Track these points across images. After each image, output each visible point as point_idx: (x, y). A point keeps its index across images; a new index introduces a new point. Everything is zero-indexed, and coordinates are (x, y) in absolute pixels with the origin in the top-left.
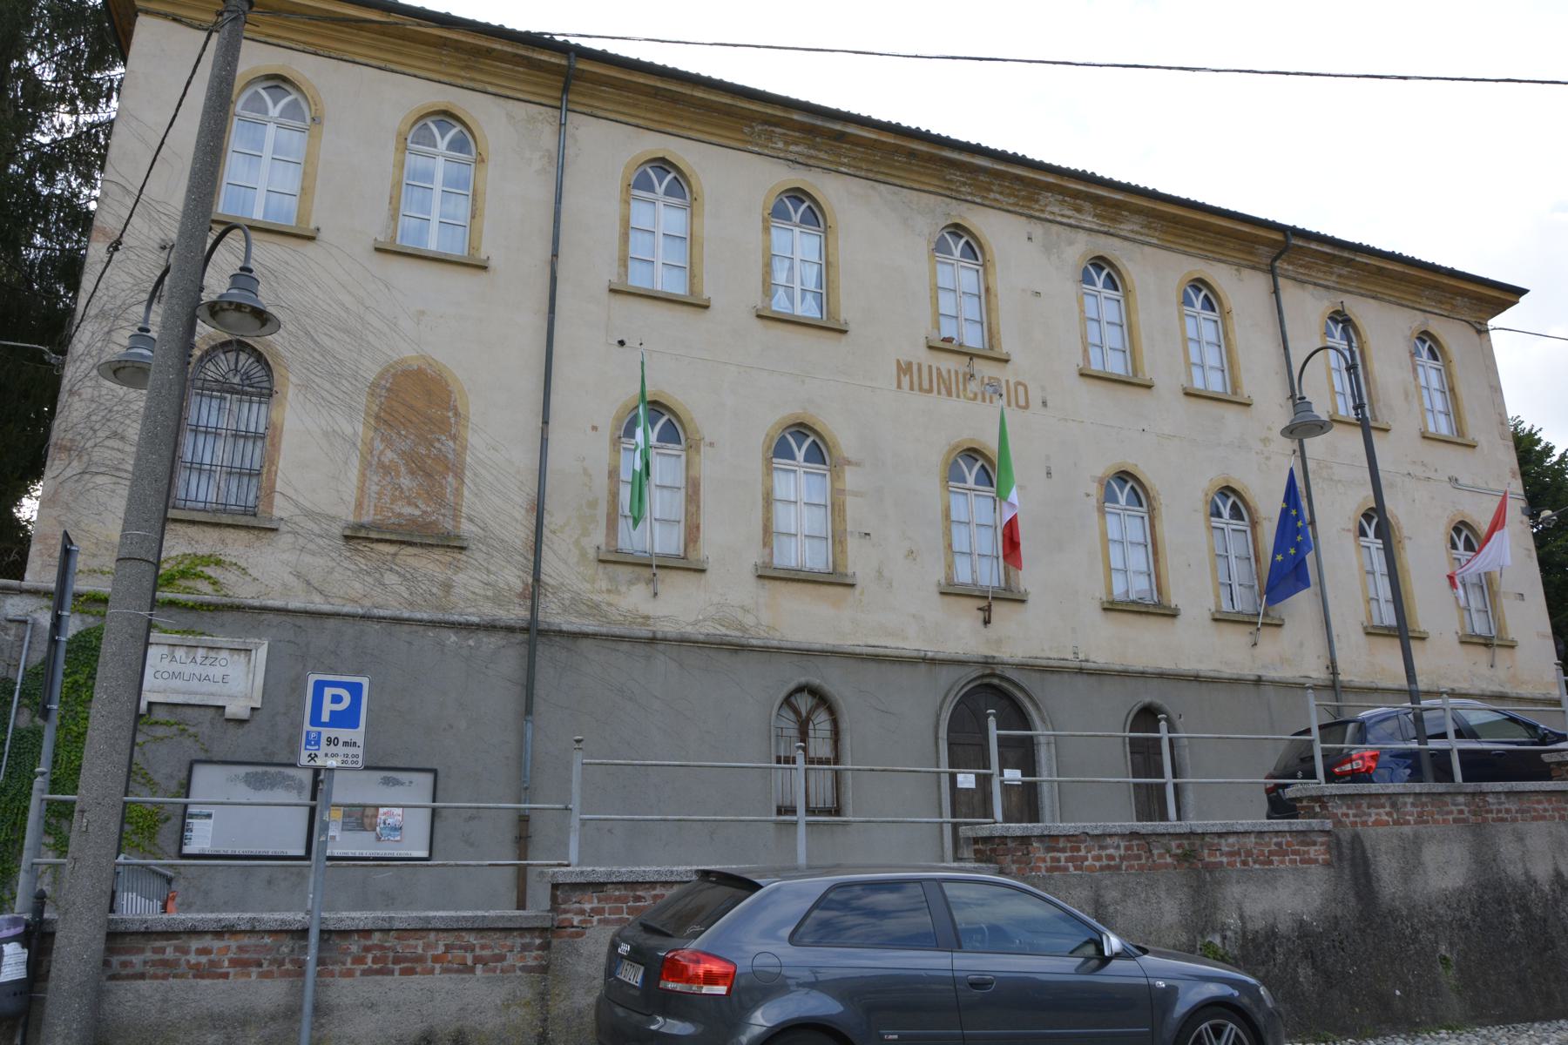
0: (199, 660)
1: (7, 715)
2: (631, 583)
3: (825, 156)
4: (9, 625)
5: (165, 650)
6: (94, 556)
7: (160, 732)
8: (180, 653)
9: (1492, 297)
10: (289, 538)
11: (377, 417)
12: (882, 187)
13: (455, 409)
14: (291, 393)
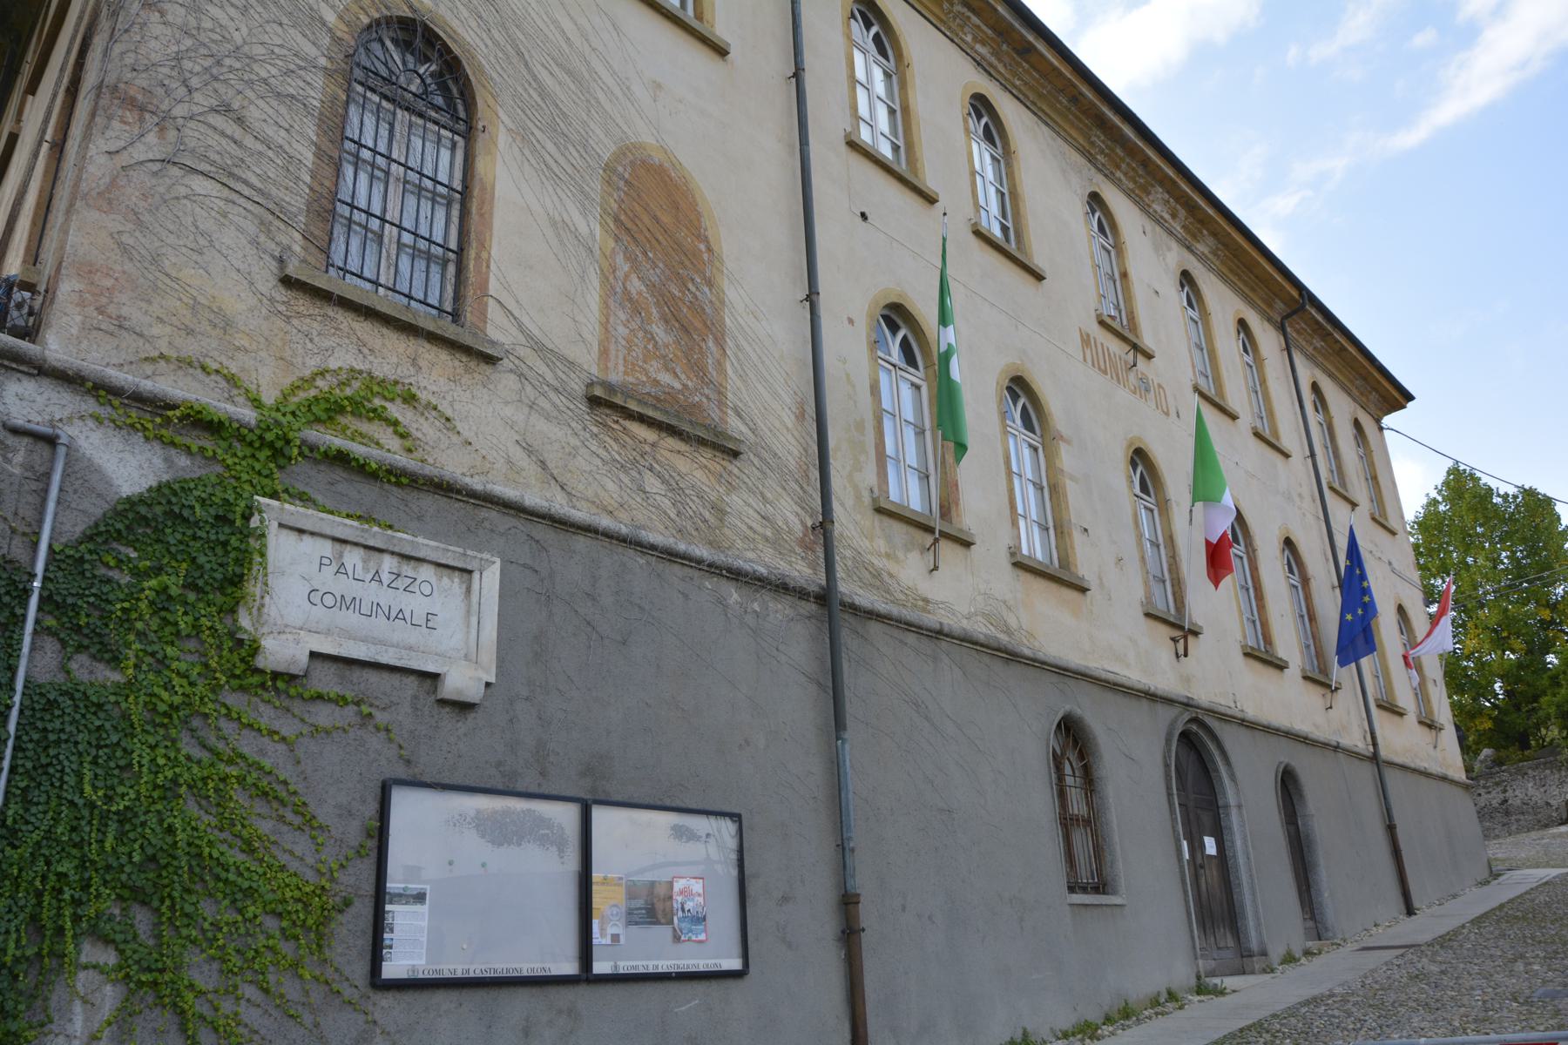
0: (386, 578)
1: (12, 649)
2: (907, 548)
3: (1002, 70)
4: (11, 440)
5: (327, 548)
6: (190, 332)
7: (324, 715)
8: (353, 557)
9: (1397, 397)
10: (511, 381)
11: (617, 220)
12: (1044, 127)
13: (706, 240)
14: (503, 139)
